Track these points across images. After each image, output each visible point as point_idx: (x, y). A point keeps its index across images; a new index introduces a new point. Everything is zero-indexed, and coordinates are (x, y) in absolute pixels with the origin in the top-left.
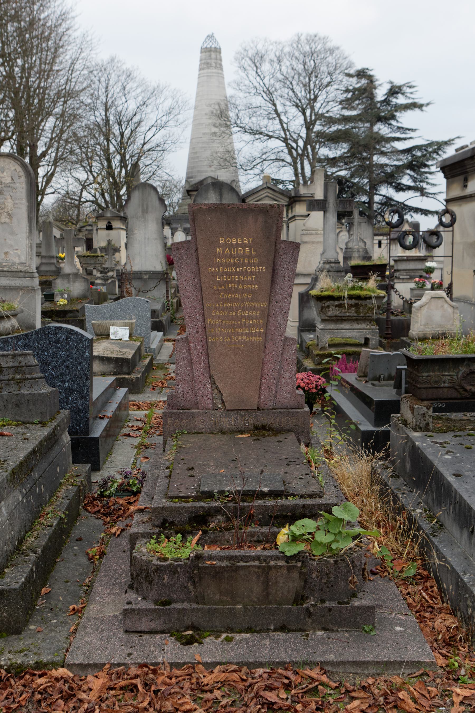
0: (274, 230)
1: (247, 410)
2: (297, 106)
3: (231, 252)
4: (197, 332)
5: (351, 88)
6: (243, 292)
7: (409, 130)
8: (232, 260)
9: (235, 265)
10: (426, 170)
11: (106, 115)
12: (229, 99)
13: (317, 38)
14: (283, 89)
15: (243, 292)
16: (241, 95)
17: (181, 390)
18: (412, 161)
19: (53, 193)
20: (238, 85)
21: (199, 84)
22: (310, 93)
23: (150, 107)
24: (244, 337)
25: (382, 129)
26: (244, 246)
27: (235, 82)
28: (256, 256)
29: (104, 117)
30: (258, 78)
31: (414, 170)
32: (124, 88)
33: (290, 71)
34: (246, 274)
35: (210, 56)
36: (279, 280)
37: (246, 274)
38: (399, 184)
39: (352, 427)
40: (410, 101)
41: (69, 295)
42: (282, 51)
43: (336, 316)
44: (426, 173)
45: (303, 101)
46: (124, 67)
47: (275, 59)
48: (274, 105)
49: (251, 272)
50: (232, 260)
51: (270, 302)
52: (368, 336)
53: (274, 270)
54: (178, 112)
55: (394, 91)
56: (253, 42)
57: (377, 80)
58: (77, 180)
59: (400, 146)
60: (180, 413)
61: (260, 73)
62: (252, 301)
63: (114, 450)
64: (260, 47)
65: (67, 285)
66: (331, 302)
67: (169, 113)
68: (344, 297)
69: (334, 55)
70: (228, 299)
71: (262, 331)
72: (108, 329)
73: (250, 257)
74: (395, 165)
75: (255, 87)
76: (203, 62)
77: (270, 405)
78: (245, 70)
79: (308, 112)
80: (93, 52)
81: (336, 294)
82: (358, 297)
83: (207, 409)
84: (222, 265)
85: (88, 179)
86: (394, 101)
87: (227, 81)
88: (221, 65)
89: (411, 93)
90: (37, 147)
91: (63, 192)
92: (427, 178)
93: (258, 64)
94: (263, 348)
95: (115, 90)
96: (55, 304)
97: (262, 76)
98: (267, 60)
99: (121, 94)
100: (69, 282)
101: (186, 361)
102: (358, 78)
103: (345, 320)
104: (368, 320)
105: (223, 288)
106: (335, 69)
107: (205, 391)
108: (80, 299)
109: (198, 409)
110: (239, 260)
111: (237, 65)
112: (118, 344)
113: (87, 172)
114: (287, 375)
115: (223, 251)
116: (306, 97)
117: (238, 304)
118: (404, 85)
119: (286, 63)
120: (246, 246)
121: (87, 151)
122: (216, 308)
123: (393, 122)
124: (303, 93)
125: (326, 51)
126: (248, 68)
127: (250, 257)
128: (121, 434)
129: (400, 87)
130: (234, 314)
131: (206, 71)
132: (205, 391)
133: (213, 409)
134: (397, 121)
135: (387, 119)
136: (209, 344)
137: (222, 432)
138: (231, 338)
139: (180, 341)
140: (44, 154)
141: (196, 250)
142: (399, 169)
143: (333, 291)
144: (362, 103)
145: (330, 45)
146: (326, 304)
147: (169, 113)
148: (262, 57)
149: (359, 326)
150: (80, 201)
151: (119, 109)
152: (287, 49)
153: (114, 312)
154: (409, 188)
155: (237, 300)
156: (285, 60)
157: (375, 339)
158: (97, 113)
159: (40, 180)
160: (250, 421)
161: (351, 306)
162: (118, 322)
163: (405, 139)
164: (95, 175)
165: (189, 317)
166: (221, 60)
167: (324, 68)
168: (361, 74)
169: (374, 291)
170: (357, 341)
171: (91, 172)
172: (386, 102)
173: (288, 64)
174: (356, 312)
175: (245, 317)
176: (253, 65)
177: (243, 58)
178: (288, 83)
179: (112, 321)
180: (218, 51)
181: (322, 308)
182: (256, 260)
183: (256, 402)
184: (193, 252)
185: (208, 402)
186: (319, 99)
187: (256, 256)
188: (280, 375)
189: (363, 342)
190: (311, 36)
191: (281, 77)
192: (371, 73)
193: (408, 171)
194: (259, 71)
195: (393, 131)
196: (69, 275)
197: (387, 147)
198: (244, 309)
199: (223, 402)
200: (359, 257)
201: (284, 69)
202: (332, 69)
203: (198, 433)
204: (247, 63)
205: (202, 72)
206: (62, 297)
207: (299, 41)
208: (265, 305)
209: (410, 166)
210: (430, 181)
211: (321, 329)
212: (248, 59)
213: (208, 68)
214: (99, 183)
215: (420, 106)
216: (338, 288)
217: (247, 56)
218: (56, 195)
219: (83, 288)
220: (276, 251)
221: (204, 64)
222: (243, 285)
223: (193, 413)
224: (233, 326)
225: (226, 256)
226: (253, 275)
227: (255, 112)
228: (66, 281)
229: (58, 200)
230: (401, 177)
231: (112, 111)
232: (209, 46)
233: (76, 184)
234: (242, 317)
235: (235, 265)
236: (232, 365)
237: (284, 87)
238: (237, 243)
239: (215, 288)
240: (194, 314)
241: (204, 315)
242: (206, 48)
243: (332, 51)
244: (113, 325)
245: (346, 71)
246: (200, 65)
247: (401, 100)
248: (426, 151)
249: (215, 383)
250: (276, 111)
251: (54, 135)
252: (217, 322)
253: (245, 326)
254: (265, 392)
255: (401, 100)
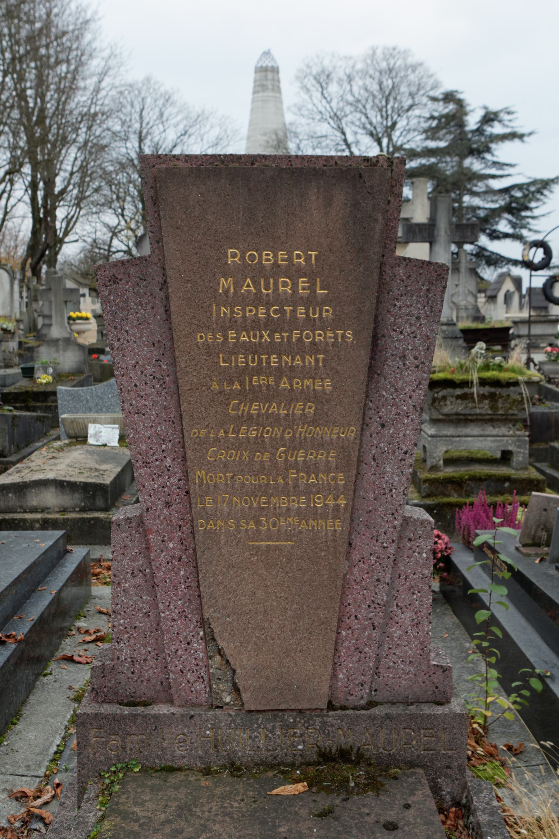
0: (378, 227)
1: (300, 711)
2: (371, 134)
3: (258, 289)
4: (168, 505)
5: (436, 114)
6: (291, 397)
7: (507, 165)
8: (262, 310)
9: (271, 325)
10: (528, 213)
11: (140, 147)
12: (288, 126)
13: (396, 52)
14: (354, 114)
15: (291, 397)
16: (303, 121)
17: (126, 653)
18: (511, 203)
19: (77, 241)
20: (300, 109)
21: (252, 110)
22: (387, 119)
23: (193, 138)
24: (293, 520)
25: (474, 164)
26: (294, 272)
27: (295, 105)
28: (326, 301)
29: (138, 150)
30: (324, 102)
31: (513, 215)
32: (161, 115)
33: (362, 92)
34: (300, 349)
35: (266, 76)
36: (391, 367)
37: (300, 349)
38: (495, 231)
39: (536, 684)
40: (508, 131)
41: (55, 370)
42: (353, 67)
43: (457, 414)
44: (528, 217)
45: (379, 130)
46: (162, 90)
47: (345, 78)
48: (344, 133)
49: (313, 343)
50: (262, 310)
51: (364, 425)
52: (510, 448)
53: (375, 338)
54: (226, 143)
55: (490, 118)
56: (318, 57)
57: (468, 105)
58: (107, 225)
59: (497, 185)
60: (123, 717)
61: (326, 95)
62: (314, 422)
63: (26, 711)
64: (326, 63)
65: (55, 355)
66: (450, 390)
67: (217, 144)
68: (472, 382)
69: (417, 72)
70: (250, 417)
71: (342, 502)
72: (86, 428)
73: (310, 301)
74: (490, 209)
75: (321, 112)
76: (257, 83)
77: (361, 695)
78: (308, 90)
79: (385, 141)
80: (122, 68)
81: (458, 377)
82: (496, 383)
83: (194, 705)
84: (233, 323)
85: (118, 224)
86: (489, 130)
87: (285, 105)
88: (279, 87)
89: (510, 121)
90: (54, 183)
91: (89, 240)
92: (528, 223)
93: (324, 85)
94: (344, 548)
95: (150, 116)
96: (35, 382)
97: (329, 99)
98: (335, 79)
99: (158, 122)
100: (57, 351)
101: (140, 579)
102: (445, 103)
103: (472, 421)
104: (510, 421)
105: (237, 386)
106: (418, 90)
107: (188, 658)
108: (73, 374)
109: (171, 702)
110: (282, 311)
111: (298, 84)
112: (98, 454)
113: (117, 216)
114: (406, 617)
115: (238, 285)
116: (382, 123)
117: (278, 432)
118: (501, 111)
119: (358, 83)
120: (301, 272)
121: (118, 190)
122: (217, 440)
123: (488, 156)
124: (379, 118)
125: (406, 68)
126: (312, 89)
127: (310, 301)
128: (59, 654)
129: (496, 114)
130: (266, 457)
131: (260, 94)
132: (188, 658)
133: (212, 707)
134: (493, 155)
135: (479, 152)
136: (199, 537)
137: (235, 769)
138: (258, 523)
139: (124, 526)
140: (63, 191)
141: (164, 284)
142: (495, 214)
143: (453, 372)
144: (450, 132)
145: (411, 60)
146: (441, 394)
147: (217, 144)
148: (328, 76)
149: (495, 431)
150: (109, 251)
151: (156, 139)
152: (359, 66)
153: (101, 398)
154: (506, 236)
155: (276, 420)
156: (357, 79)
157: (521, 454)
158: (129, 145)
159: (58, 225)
160: (305, 741)
161: (482, 397)
162: (103, 416)
163: (501, 176)
164: (128, 220)
165: (146, 464)
166: (279, 81)
167: (404, 89)
168: (449, 97)
169: (521, 373)
170: (489, 454)
171: (123, 215)
172: (479, 131)
173: (361, 83)
174: (492, 408)
175: (295, 465)
176: (318, 86)
177: (305, 77)
178: (360, 106)
179: (95, 415)
180: (275, 70)
181: (434, 400)
182: (328, 312)
183: (325, 690)
184: (156, 289)
185: (199, 686)
186: (398, 126)
187: (326, 301)
188: (389, 617)
189: (498, 455)
190: (388, 49)
191: (350, 98)
192: (461, 96)
193: (506, 215)
194: (325, 92)
195: (487, 166)
196: (57, 341)
197: (480, 187)
198: (294, 445)
199: (236, 689)
200: (468, 317)
201: (355, 89)
202: (414, 89)
203: (171, 770)
204: (310, 82)
205: (256, 95)
206: (46, 372)
207: (374, 53)
208: (352, 433)
209: (508, 209)
210: (532, 227)
211: (432, 436)
212: (311, 78)
213: (264, 91)
214: (132, 230)
215: (521, 137)
216: (461, 366)
217: (311, 74)
218: (80, 244)
219: (77, 359)
220: (382, 287)
221: (259, 86)
222: (290, 379)
223: (156, 717)
224: (265, 490)
225: (244, 301)
226: (317, 352)
227: (320, 143)
228: (53, 349)
229: (83, 249)
230: (497, 223)
231: (147, 142)
232: (264, 65)
233: (105, 230)
234: (288, 466)
235: (271, 325)
236: (260, 594)
237: (356, 111)
238: (276, 265)
239: (215, 387)
240: (159, 455)
241: (184, 459)
242: (262, 67)
243: (414, 68)
244: (95, 421)
245: (432, 93)
246: (255, 87)
247: (497, 129)
248: (528, 190)
249: (214, 639)
250: (345, 141)
251: (75, 169)
252: (221, 478)
253: (295, 490)
254: (349, 663)
255: (497, 129)
